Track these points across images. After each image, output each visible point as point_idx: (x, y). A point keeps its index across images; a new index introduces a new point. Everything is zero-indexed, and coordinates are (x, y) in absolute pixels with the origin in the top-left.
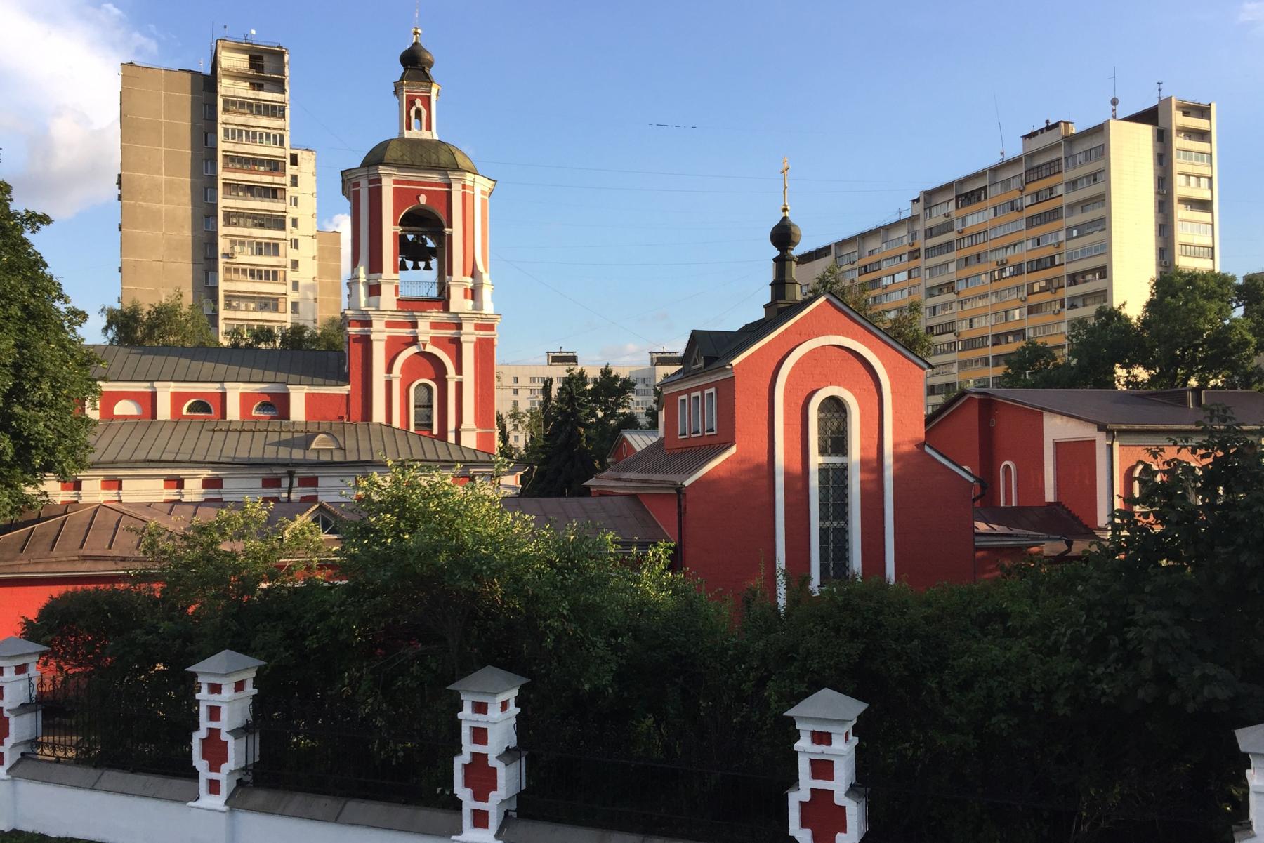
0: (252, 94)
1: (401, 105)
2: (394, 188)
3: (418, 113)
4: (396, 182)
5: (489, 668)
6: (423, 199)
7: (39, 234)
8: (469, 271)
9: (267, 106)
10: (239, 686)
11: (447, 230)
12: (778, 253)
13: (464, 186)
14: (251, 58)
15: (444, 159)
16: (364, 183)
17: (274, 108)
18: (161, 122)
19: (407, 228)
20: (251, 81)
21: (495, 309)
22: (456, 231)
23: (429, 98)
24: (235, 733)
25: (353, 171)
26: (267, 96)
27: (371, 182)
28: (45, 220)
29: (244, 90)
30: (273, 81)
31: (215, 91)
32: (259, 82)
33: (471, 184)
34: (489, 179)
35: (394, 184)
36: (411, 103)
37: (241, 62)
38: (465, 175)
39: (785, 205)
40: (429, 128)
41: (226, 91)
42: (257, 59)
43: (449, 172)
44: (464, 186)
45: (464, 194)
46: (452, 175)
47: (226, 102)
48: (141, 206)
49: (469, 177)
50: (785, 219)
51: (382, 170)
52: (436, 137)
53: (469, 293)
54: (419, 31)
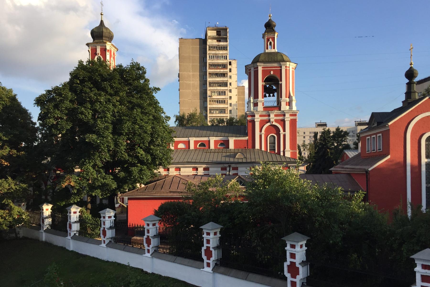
1: (265, 41)
3: (270, 43)
4: (263, 68)
5: (296, 233)
6: (272, 73)
7: (157, 93)
8: (288, 96)
11: (280, 82)
12: (407, 81)
13: (286, 67)
14: (217, 32)
15: (279, 58)
16: (252, 69)
17: (224, 47)
19: (267, 83)
21: (297, 108)
22: (283, 83)
23: (274, 38)
26: (222, 43)
27: (254, 68)
28: (158, 89)
29: (215, 43)
31: (206, 44)
32: (219, 39)
34: (295, 63)
36: (268, 40)
38: (286, 63)
40: (274, 48)
42: (218, 33)
44: (286, 67)
45: (286, 69)
46: (282, 63)
47: (209, 47)
49: (288, 63)
50: (411, 68)
52: (276, 51)
54: (271, 15)
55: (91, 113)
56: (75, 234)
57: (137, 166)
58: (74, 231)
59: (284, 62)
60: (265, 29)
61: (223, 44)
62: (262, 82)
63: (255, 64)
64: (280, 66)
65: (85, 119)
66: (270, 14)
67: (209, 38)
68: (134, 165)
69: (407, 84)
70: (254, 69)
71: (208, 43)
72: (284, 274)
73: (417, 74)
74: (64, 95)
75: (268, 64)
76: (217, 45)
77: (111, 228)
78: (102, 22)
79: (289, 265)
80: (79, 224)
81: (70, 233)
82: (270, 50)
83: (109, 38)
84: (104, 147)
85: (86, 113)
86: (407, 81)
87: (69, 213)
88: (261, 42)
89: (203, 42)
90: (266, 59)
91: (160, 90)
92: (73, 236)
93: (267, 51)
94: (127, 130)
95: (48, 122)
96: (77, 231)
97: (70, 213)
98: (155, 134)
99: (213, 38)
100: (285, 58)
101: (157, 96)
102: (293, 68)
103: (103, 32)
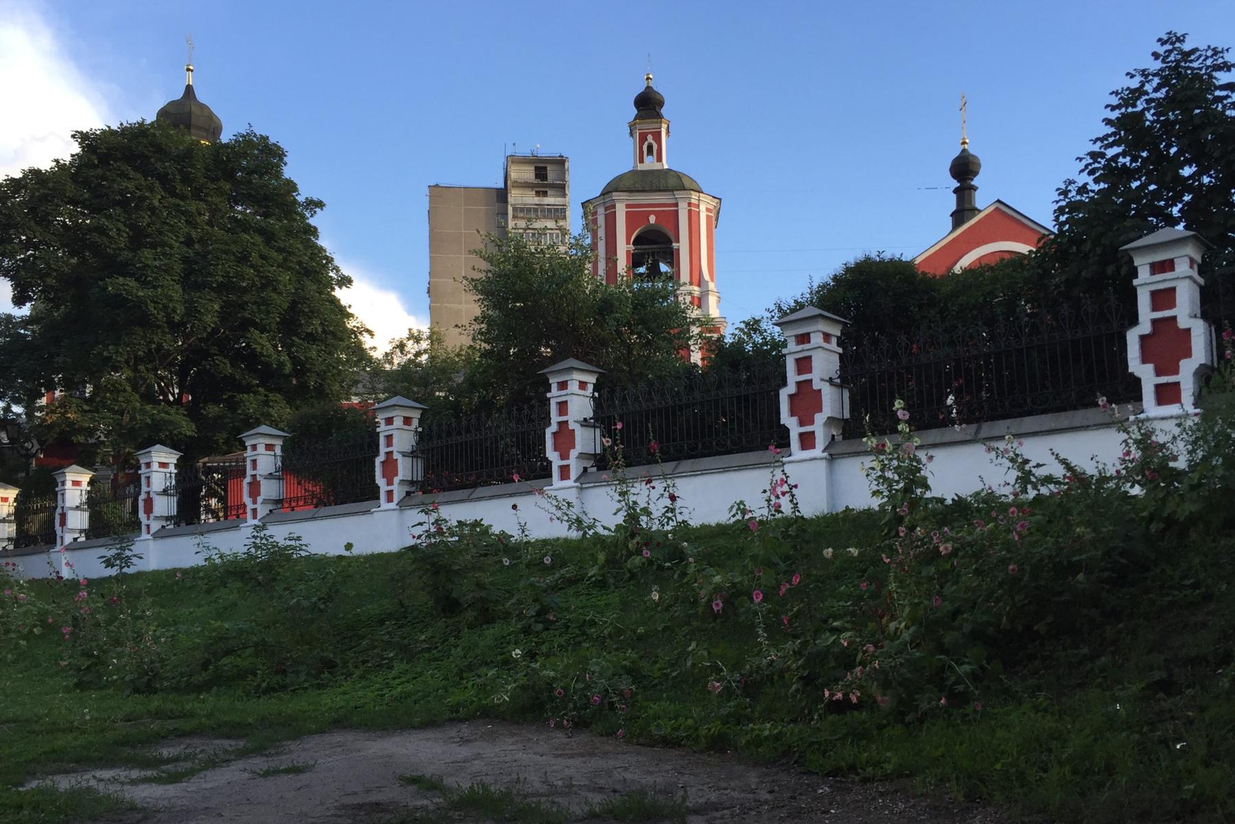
0: (536, 200)
1: (635, 143)
2: (626, 212)
3: (650, 148)
4: (628, 206)
5: (571, 359)
6: (652, 219)
7: (316, 216)
8: (695, 280)
9: (551, 209)
10: (407, 421)
11: (675, 245)
12: (956, 184)
13: (690, 204)
14: (536, 168)
15: (672, 182)
16: (601, 211)
17: (556, 210)
18: (461, 234)
19: (639, 247)
20: (537, 189)
21: (720, 313)
22: (683, 246)
23: (660, 133)
24: (404, 454)
25: (593, 201)
26: (550, 200)
27: (606, 209)
28: (320, 204)
29: (530, 199)
30: (558, 188)
31: (506, 201)
32: (543, 189)
33: (696, 202)
34: (714, 197)
35: (626, 208)
36: (643, 138)
37: (528, 174)
38: (691, 194)
39: (964, 139)
40: (659, 159)
41: (515, 200)
42: (541, 173)
43: (675, 192)
44: (690, 204)
45: (690, 211)
46: (679, 194)
47: (515, 209)
48: (446, 307)
49: (694, 196)
50: (964, 150)
51: (615, 195)
52: (666, 167)
53: (696, 302)
54: (651, 76)
55: (126, 233)
56: (75, 539)
57: (256, 393)
58: (73, 530)
59: (684, 192)
60: (635, 112)
61: (553, 203)
62: (628, 243)
63: (606, 196)
64: (673, 201)
65: (110, 248)
66: (648, 74)
67: (513, 187)
68: (248, 389)
69: (956, 191)
70: (606, 211)
71: (511, 200)
72: (545, 455)
73: (979, 165)
74: (54, 182)
75: (640, 196)
76: (536, 205)
77: (165, 492)
78: (189, 90)
79: (554, 431)
80: (86, 515)
81: (62, 537)
82: (650, 163)
83: (208, 130)
84: (155, 308)
85: (111, 230)
86: (956, 184)
87: (60, 484)
88: (628, 146)
89: (502, 195)
90: (637, 185)
91: (324, 205)
92: (71, 543)
93: (640, 167)
94: (222, 276)
95: (8, 251)
96: (81, 531)
97: (63, 483)
98: (305, 303)
99: (526, 185)
100: (687, 184)
101: (316, 220)
102: (708, 210)
103: (190, 113)
